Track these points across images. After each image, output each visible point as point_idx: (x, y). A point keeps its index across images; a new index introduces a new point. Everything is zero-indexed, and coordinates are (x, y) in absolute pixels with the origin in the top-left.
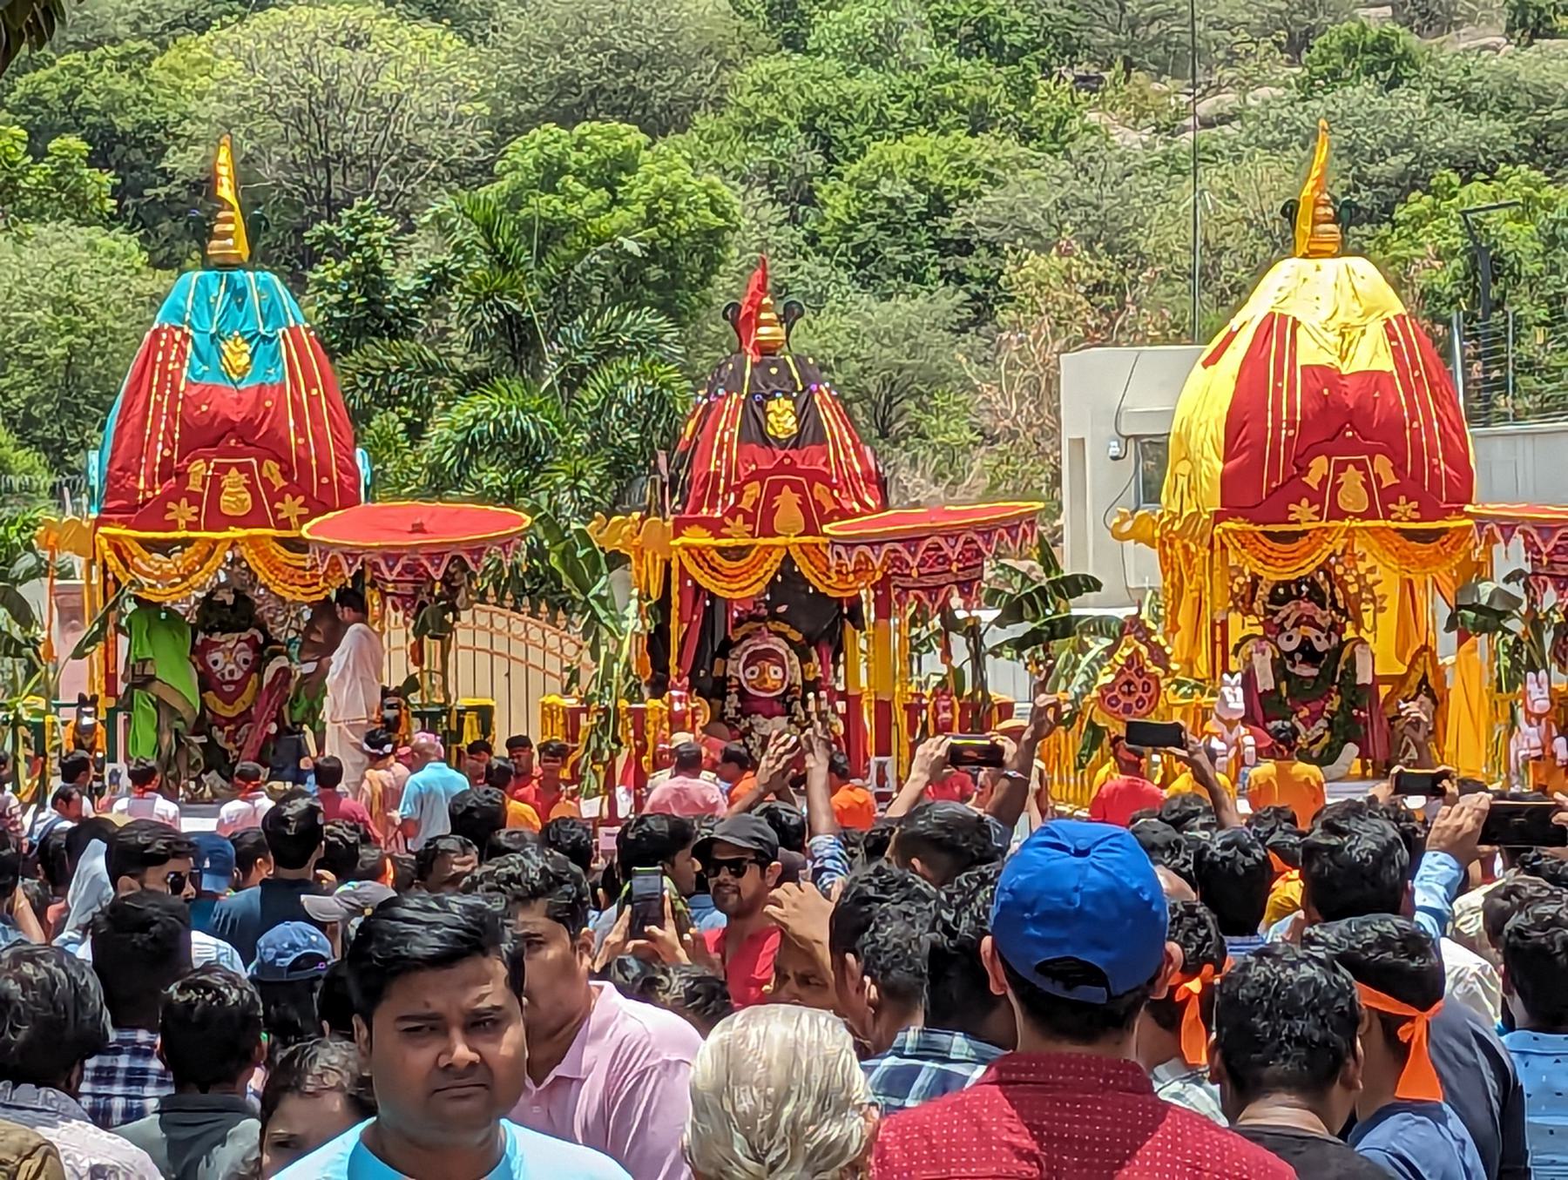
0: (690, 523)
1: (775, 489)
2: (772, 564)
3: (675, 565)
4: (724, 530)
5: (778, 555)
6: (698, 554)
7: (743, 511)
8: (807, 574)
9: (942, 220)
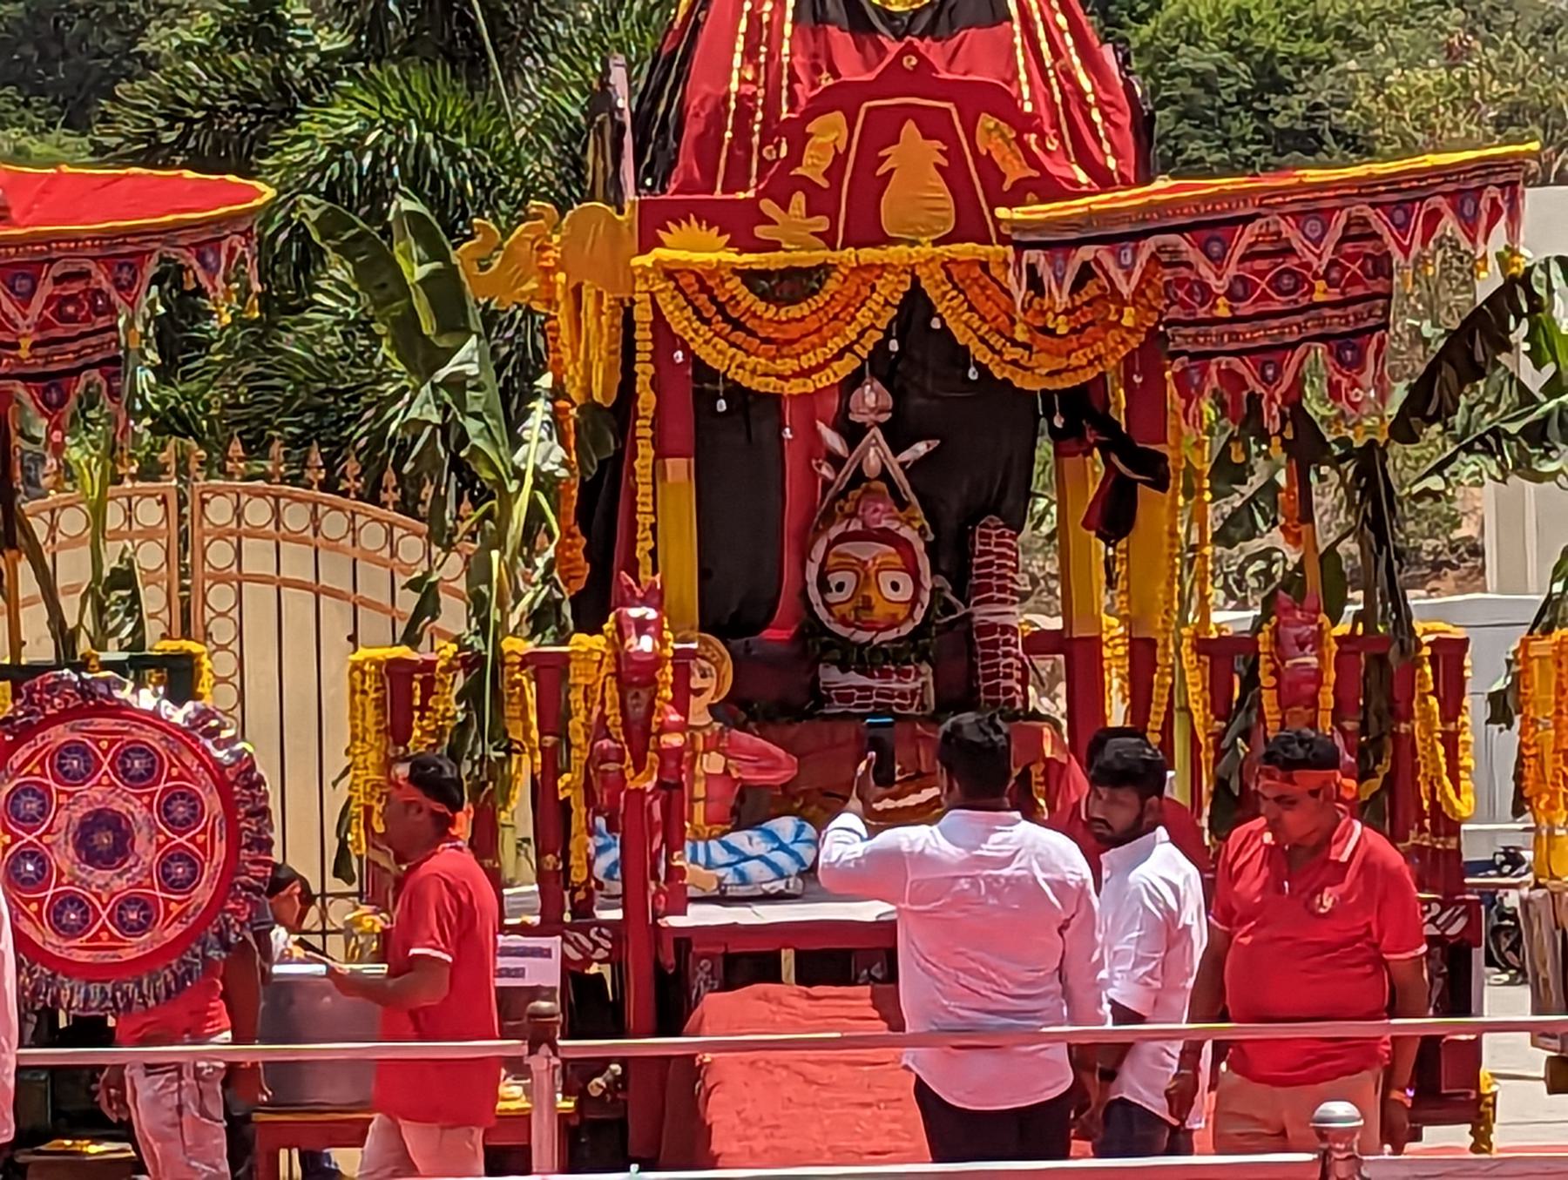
0: (679, 213)
1: (881, 132)
2: (876, 314)
3: (643, 315)
4: (761, 231)
5: (891, 289)
6: (698, 286)
7: (806, 184)
8: (962, 336)
9: (1276, 101)
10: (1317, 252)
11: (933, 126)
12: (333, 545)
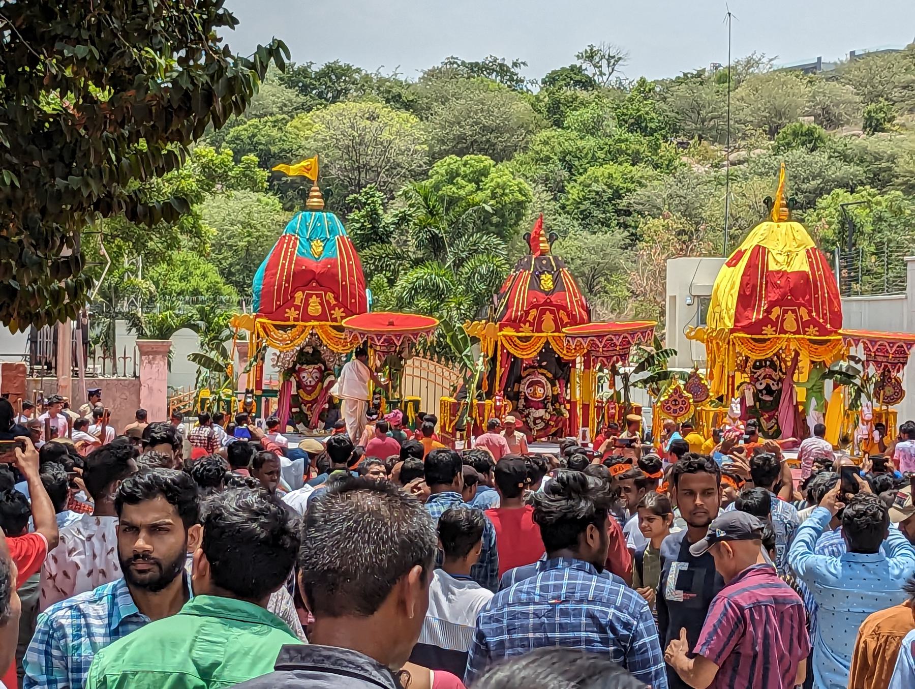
2: (541, 344)
3: (499, 343)
5: (543, 340)
6: (509, 339)
7: (529, 321)
8: (555, 349)
10: (618, 341)
11: (552, 312)
12: (424, 369)
